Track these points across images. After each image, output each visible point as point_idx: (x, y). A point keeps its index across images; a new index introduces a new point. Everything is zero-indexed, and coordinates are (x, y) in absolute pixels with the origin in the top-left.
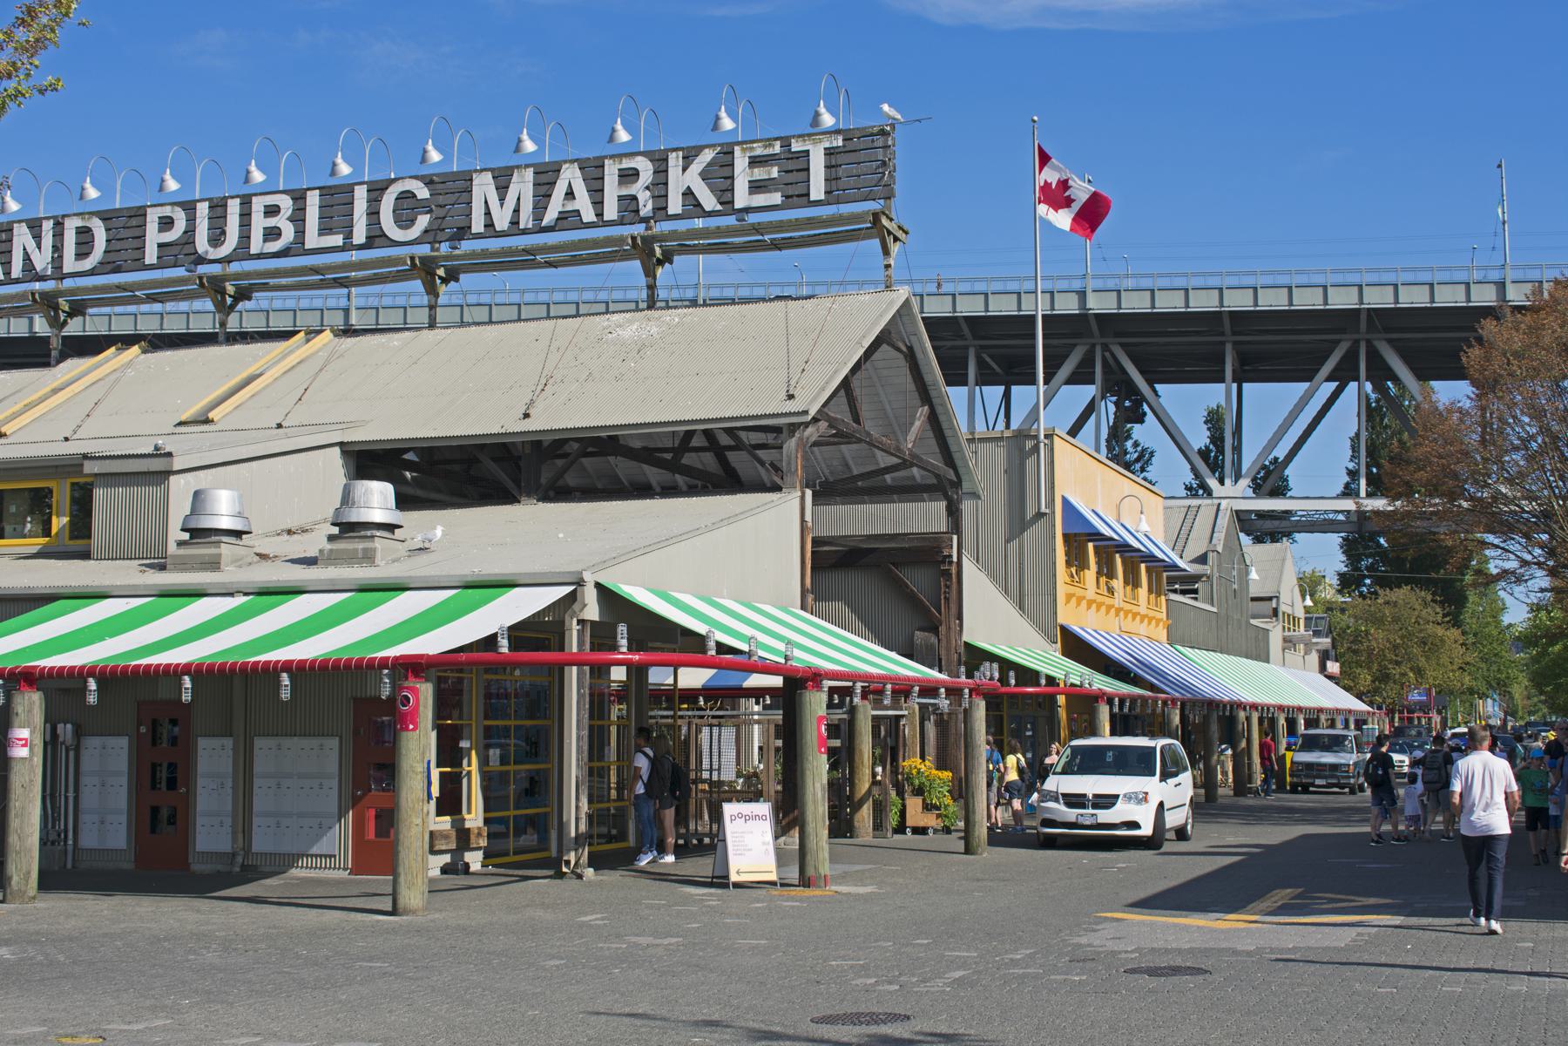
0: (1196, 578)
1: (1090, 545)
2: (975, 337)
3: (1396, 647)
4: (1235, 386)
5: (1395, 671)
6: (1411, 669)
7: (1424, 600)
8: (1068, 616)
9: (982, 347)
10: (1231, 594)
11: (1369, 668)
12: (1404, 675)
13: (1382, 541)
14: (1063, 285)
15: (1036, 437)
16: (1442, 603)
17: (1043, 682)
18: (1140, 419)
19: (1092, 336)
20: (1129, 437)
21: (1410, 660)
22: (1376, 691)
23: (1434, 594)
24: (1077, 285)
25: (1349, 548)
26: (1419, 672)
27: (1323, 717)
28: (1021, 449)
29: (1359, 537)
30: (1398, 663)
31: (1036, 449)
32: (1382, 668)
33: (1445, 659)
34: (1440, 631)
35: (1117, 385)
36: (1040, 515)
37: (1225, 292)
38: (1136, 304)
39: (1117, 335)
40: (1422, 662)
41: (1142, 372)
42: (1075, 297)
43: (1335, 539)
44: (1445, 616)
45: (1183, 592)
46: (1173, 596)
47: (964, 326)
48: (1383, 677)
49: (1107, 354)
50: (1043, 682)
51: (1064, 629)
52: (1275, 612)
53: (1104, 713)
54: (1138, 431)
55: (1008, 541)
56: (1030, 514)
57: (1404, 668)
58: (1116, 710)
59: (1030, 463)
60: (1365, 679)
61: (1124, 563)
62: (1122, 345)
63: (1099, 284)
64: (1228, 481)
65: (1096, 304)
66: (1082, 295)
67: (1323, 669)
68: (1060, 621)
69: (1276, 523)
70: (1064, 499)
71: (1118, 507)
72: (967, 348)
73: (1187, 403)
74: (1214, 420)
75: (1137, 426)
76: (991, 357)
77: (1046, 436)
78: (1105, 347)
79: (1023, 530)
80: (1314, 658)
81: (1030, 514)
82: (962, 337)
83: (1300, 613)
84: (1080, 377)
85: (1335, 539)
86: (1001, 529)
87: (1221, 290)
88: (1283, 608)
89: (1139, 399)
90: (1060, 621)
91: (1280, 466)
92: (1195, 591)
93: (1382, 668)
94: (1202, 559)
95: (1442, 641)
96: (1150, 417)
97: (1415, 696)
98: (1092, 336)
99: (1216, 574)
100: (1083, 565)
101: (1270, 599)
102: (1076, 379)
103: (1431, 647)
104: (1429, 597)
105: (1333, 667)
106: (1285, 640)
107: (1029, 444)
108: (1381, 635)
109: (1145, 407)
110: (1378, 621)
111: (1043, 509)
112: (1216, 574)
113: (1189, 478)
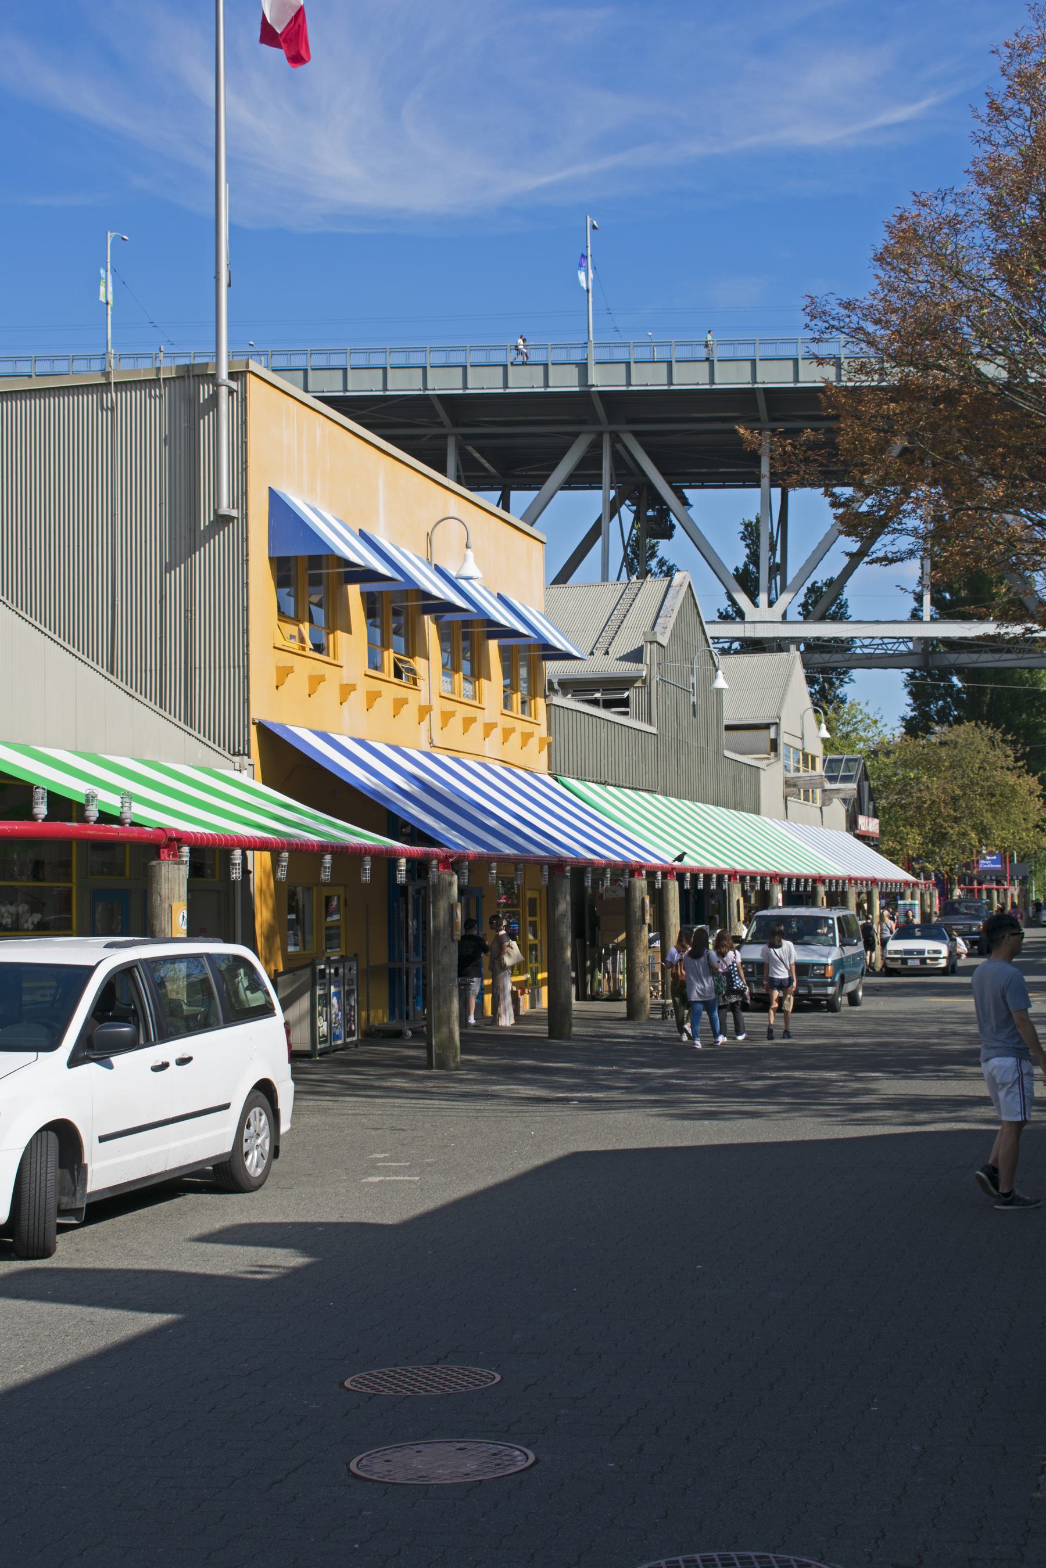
0: (627, 683)
1: (493, 645)
2: (456, 424)
3: (955, 799)
4: (776, 492)
5: (953, 832)
6: (974, 827)
7: (991, 739)
8: (266, 706)
9: (465, 436)
10: (686, 712)
11: (921, 826)
12: (964, 834)
13: (955, 680)
14: (560, 355)
15: (213, 378)
16: (1014, 743)
17: (41, 810)
18: (667, 533)
19: (597, 422)
20: (653, 555)
21: (972, 815)
22: (929, 856)
23: (1005, 733)
24: (577, 356)
25: (919, 693)
26: (983, 831)
27: (822, 890)
28: (191, 400)
29: (929, 671)
30: (956, 820)
31: (214, 400)
32: (936, 827)
33: (1016, 815)
34: (1011, 779)
35: (633, 488)
36: (222, 521)
37: (759, 364)
38: (649, 379)
39: (629, 422)
40: (988, 818)
41: (664, 474)
42: (574, 371)
43: (898, 677)
44: (1017, 760)
45: (608, 704)
46: (557, 700)
47: (438, 406)
48: (939, 838)
49: (619, 447)
50: (41, 810)
51: (263, 730)
52: (774, 746)
53: (173, 880)
54: (664, 548)
55: (169, 568)
56: (205, 518)
57: (966, 825)
58: (687, 886)
59: (205, 424)
60: (914, 839)
61: (443, 637)
62: (636, 434)
63: (604, 355)
64: (763, 598)
65: (602, 380)
66: (583, 368)
67: (852, 825)
68: (257, 713)
69: (826, 657)
70: (275, 498)
71: (429, 537)
72: (445, 437)
73: (720, 513)
74: (751, 533)
75: (663, 543)
76: (477, 449)
77: (232, 376)
78: (616, 438)
79: (192, 549)
80: (838, 810)
81: (205, 518)
82: (441, 425)
83: (816, 749)
84: (583, 478)
85: (898, 677)
86: (153, 545)
87: (753, 362)
88: (784, 739)
89: (664, 511)
90: (257, 713)
91: (837, 584)
92: (625, 702)
93: (936, 827)
94: (636, 656)
95: (1014, 791)
96: (678, 531)
97: (988, 863)
98: (597, 422)
99: (656, 677)
100: (478, 672)
101: (767, 727)
102: (577, 481)
103: (999, 799)
104: (998, 736)
105: (869, 824)
106: (788, 783)
107: (205, 391)
108: (935, 783)
109: (672, 516)
110: (932, 766)
111: (225, 509)
112: (656, 677)
113: (724, 604)
